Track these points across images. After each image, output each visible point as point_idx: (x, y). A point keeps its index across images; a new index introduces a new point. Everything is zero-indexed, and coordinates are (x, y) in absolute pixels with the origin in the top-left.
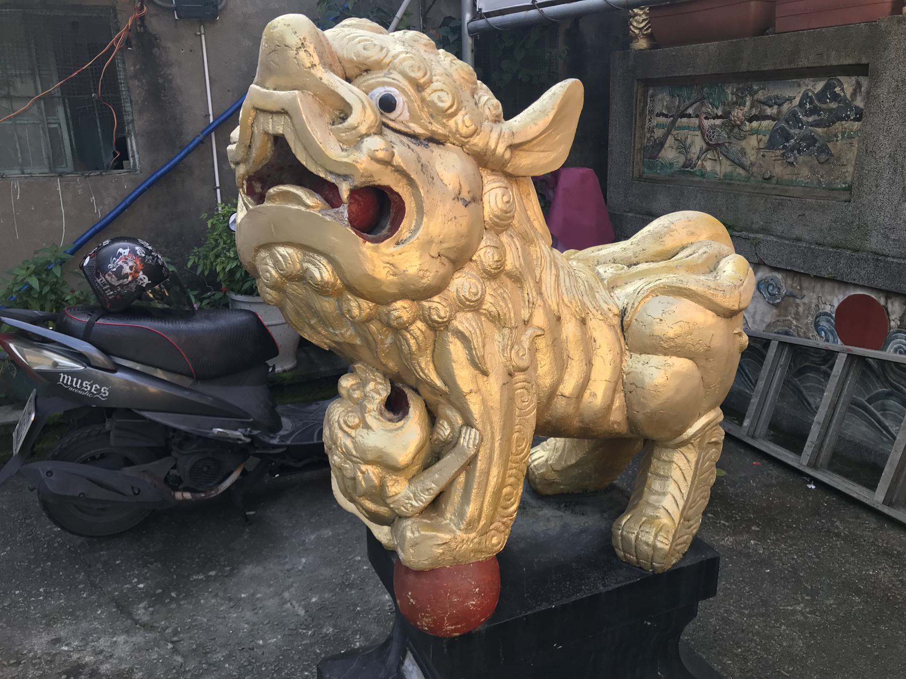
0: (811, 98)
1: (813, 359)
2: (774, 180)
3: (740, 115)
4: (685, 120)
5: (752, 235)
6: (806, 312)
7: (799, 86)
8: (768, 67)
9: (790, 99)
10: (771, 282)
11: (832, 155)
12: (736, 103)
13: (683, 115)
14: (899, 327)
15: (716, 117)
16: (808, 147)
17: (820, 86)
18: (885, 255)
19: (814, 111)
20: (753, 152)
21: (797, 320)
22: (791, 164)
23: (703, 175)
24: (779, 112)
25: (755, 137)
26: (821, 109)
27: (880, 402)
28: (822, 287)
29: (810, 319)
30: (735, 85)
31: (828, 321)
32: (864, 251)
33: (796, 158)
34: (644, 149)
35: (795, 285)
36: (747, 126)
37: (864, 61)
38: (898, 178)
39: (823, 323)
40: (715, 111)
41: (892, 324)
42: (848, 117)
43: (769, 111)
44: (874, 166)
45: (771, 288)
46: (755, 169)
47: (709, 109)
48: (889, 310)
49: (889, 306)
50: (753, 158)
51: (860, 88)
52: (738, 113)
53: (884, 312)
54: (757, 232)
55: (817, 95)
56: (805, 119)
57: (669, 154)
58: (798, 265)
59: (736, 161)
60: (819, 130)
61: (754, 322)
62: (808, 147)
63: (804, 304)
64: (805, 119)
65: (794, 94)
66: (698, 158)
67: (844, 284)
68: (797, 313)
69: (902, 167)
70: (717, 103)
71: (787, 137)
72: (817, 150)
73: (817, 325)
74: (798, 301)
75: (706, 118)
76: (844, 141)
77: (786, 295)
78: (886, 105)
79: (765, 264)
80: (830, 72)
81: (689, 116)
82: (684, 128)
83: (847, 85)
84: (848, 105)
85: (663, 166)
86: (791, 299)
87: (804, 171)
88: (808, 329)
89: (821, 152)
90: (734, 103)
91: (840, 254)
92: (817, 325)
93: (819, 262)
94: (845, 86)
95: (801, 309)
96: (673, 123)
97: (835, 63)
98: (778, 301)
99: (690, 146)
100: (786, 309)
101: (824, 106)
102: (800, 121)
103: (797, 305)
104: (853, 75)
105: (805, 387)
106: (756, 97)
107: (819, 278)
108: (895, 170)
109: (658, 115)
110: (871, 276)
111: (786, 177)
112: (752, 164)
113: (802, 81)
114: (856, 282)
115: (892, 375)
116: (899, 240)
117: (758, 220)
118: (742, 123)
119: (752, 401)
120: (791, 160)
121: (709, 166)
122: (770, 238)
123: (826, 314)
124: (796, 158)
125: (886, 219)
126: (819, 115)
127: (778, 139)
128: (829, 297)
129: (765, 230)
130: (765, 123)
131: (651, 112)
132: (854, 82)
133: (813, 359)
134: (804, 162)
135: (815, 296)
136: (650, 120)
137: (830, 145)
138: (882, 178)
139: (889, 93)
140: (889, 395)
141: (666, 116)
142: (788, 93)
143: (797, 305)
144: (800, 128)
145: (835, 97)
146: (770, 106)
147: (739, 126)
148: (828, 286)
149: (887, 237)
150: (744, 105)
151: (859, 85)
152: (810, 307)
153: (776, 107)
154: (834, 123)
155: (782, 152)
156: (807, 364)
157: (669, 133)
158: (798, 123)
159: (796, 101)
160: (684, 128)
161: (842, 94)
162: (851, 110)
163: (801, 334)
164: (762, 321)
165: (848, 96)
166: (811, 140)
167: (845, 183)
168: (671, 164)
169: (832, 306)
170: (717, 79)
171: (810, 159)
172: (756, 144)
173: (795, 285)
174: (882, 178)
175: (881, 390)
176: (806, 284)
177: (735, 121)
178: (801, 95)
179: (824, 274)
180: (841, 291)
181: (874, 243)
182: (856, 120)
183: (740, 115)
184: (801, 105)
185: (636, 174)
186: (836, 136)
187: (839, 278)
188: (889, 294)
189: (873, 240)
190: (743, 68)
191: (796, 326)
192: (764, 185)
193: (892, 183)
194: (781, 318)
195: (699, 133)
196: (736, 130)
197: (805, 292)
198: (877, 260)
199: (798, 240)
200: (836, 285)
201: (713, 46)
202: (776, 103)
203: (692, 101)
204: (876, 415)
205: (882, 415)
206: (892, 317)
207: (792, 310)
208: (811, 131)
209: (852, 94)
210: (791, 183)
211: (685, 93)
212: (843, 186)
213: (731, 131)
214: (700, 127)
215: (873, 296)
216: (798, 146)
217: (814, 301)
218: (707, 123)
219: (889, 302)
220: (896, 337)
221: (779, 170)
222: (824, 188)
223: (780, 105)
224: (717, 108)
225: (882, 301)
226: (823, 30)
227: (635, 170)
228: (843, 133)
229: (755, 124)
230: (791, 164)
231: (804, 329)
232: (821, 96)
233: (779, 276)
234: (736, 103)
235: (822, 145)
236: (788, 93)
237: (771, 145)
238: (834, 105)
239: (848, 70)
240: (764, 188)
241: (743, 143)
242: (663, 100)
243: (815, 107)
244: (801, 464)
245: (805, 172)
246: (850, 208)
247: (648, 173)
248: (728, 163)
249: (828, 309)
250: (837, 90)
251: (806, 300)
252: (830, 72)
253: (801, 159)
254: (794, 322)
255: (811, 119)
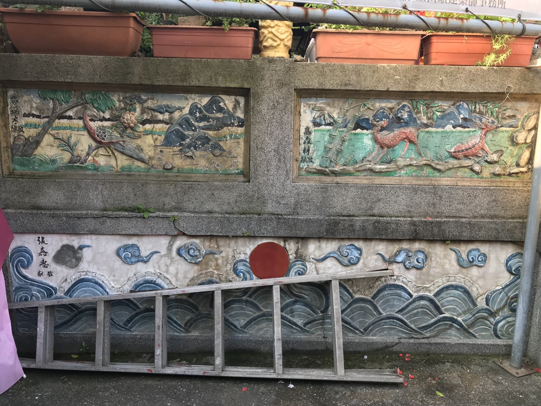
0: (200, 109)
1: (236, 294)
2: (175, 170)
3: (133, 118)
4: (64, 122)
5: (169, 214)
6: (225, 263)
7: (187, 99)
8: (161, 81)
9: (180, 109)
10: (190, 247)
11: (224, 150)
12: (125, 109)
13: (61, 117)
14: (295, 258)
15: (104, 119)
16: (203, 144)
17: (205, 100)
18: (350, 216)
19: (204, 118)
20: (150, 148)
21: (218, 270)
22: (191, 157)
23: (96, 169)
24: (171, 118)
25: (150, 137)
26: (209, 118)
27: (289, 308)
28: (236, 242)
29: (229, 267)
30: (121, 94)
31: (245, 265)
32: (264, 213)
33: (193, 153)
34: (12, 148)
35: (212, 245)
36: (141, 128)
37: (246, 86)
38: (282, 165)
39: (241, 267)
40: (102, 114)
41: (291, 257)
42: (233, 124)
43: (160, 117)
44: (264, 157)
45: (191, 252)
46: (154, 162)
47: (95, 112)
48: (287, 249)
49: (287, 247)
50: (151, 153)
51: (239, 104)
52: (131, 117)
53: (284, 251)
54: (169, 211)
55: (204, 107)
56: (196, 124)
57: (48, 150)
58: (216, 230)
59: (135, 156)
60: (211, 133)
61: (177, 280)
62: (203, 144)
63: (222, 257)
64: (196, 124)
65: (184, 105)
66: (88, 154)
67: (254, 237)
68: (217, 265)
69: (284, 158)
70: (103, 108)
71: (183, 137)
72: (211, 147)
73: (235, 270)
74: (216, 256)
75: (91, 120)
76: (232, 141)
77: (206, 254)
78: (268, 117)
79: (184, 234)
80: (213, 91)
81: (70, 118)
82: (65, 128)
83: (228, 102)
84: (231, 116)
85: (42, 162)
86: (211, 256)
87: (202, 161)
88: (228, 274)
89: (215, 148)
90: (122, 109)
91: (250, 218)
92: (235, 270)
93: (234, 226)
94: (227, 102)
95: (220, 262)
96: (50, 123)
97: (222, 85)
98: (200, 260)
99: (76, 144)
100: (207, 264)
101: (212, 115)
102: (193, 125)
103: (217, 259)
104: (232, 95)
105: (231, 315)
106: (145, 105)
107: (236, 237)
108: (280, 160)
109: (25, 115)
110: (276, 230)
111: (186, 167)
112: (150, 158)
113: (189, 96)
114: (265, 235)
115: (295, 289)
116: (287, 204)
117: (169, 202)
118: (135, 125)
119: (216, 342)
120: (190, 154)
121: (102, 161)
122: (186, 214)
123: (242, 261)
124: (193, 153)
125: (278, 192)
126: (208, 122)
127: (174, 138)
128: (242, 249)
129: (177, 209)
130: (159, 126)
131: (15, 112)
132: (233, 100)
133: (236, 294)
134: (201, 156)
135: (231, 250)
136: (15, 120)
137: (221, 144)
138: (271, 165)
139: (268, 109)
140: (295, 302)
141: (38, 117)
142: (176, 103)
143: (217, 259)
144: (193, 130)
145: (220, 110)
146: (161, 113)
147: (132, 128)
148: (240, 241)
149: (279, 203)
150: (135, 110)
151: (237, 103)
152: (228, 258)
153: (167, 114)
154: (222, 128)
155: (179, 148)
156: (231, 299)
157: (45, 131)
158: (191, 126)
159: (186, 111)
160: (65, 128)
161: (226, 108)
162: (234, 119)
163: (223, 279)
164: (185, 277)
165: (231, 109)
166: (207, 140)
167: (238, 169)
168: (53, 161)
169: (245, 254)
170: (101, 89)
171: (205, 153)
172: (152, 142)
173: (212, 245)
174: (271, 165)
175: (288, 301)
176: (222, 242)
177: (129, 124)
178: (189, 106)
179: (239, 233)
180: (252, 242)
181: (270, 207)
182: (239, 126)
183: (133, 118)
184: (191, 112)
185: (6, 172)
186: (225, 137)
187: (252, 235)
188: (286, 239)
189: (269, 206)
190: (136, 80)
191: (218, 274)
192: (166, 174)
193: (278, 168)
194: (204, 272)
195: (85, 133)
196: (129, 131)
197: (222, 249)
198: (279, 218)
199: (210, 212)
200: (247, 239)
201: (97, 59)
202: (167, 111)
203: (70, 104)
204: (287, 318)
205: (291, 316)
206: (290, 253)
207: (213, 264)
208: (205, 134)
209: (233, 109)
210: (191, 171)
211: (61, 96)
212: (237, 171)
213: (123, 131)
214: (86, 128)
215: (275, 242)
216: (193, 144)
217: (231, 254)
218: (94, 125)
219: (287, 243)
220: (295, 265)
221: (178, 162)
222: (221, 174)
223: (171, 113)
224: (104, 112)
225: (282, 244)
226: (210, 60)
227: (4, 168)
228: (231, 136)
229: (148, 126)
230: (191, 157)
231: (225, 275)
232: (208, 107)
233: (197, 241)
234: (125, 109)
235: (215, 143)
236: (176, 103)
237: (168, 142)
238: (220, 115)
239: (228, 91)
240: (167, 176)
241: (139, 142)
242: (30, 102)
243: (205, 116)
244: (278, 374)
245: (203, 163)
246: (251, 187)
247: (19, 169)
248: (124, 157)
249: (242, 257)
250: (222, 104)
251: (223, 254)
252: (213, 91)
253: (198, 153)
254: (216, 272)
255: (202, 124)
